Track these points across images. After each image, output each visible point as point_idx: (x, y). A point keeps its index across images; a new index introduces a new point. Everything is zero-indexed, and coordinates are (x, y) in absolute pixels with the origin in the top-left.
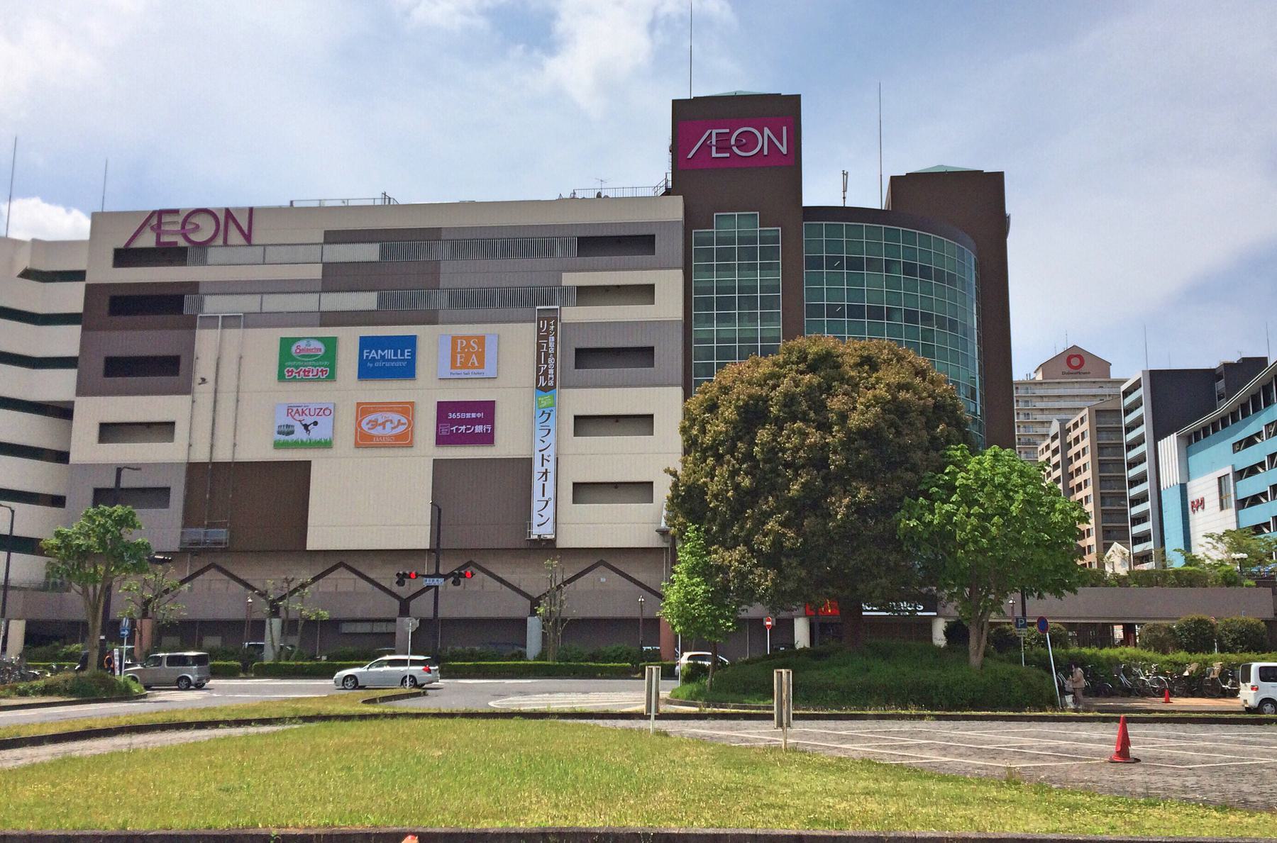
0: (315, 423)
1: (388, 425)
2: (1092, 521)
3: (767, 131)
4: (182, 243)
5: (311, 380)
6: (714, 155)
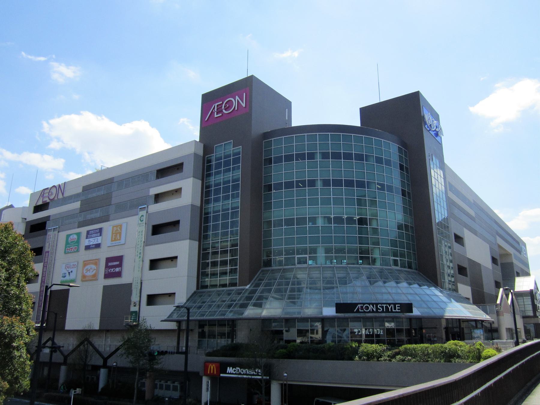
0: (72, 272)
1: (91, 271)
2: (447, 281)
3: (237, 98)
4: (48, 201)
5: (73, 252)
6: (216, 116)
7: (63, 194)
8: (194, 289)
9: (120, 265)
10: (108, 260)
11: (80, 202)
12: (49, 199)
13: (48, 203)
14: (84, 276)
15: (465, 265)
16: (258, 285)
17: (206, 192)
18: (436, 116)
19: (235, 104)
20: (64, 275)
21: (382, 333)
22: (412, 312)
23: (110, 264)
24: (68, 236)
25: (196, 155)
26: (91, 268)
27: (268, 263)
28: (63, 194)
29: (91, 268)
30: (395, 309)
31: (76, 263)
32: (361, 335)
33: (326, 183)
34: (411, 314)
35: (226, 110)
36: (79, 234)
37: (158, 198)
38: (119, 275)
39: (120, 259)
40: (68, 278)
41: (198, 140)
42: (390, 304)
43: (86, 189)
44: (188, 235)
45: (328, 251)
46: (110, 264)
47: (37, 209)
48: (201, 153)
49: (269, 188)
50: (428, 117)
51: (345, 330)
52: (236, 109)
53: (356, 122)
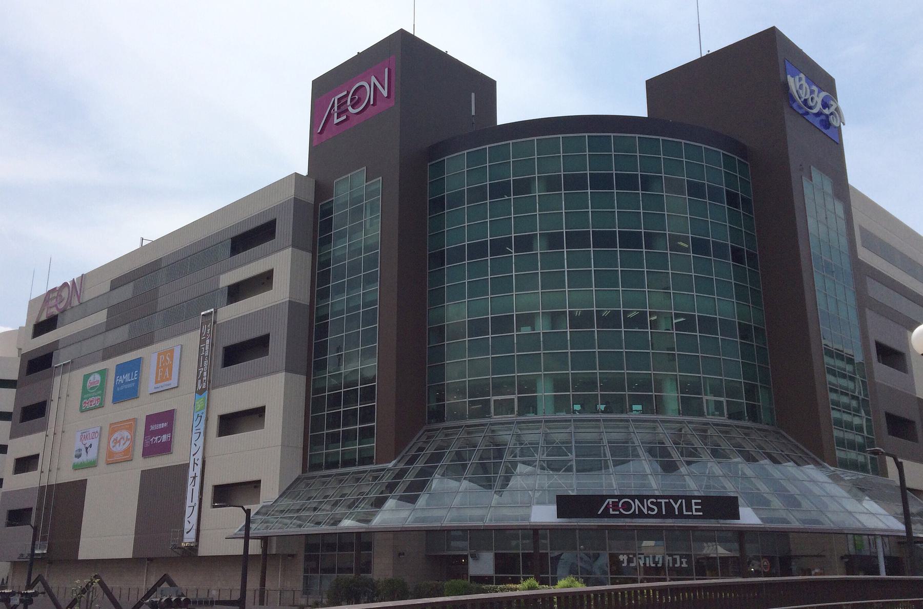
0: (91, 446)
1: (122, 442)
6: (336, 121)
7: (79, 297)
8: (298, 471)
9: (169, 430)
10: (151, 419)
11: (105, 311)
12: (58, 309)
13: (57, 316)
14: (110, 454)
15: (912, 414)
16: (412, 461)
17: (321, 277)
18: (826, 83)
19: (369, 93)
20: (78, 453)
21: (684, 565)
22: (736, 516)
23: (153, 428)
24: (86, 377)
25: (297, 202)
26: (122, 438)
27: (438, 415)
28: (79, 297)
29: (122, 438)
30: (689, 508)
31: (99, 430)
32: (635, 569)
33: (554, 241)
34: (736, 521)
35: (353, 107)
36: (103, 373)
37: (236, 292)
38: (166, 448)
39: (168, 417)
40: (84, 458)
41: (304, 172)
42: (676, 498)
43: (116, 284)
44: (282, 363)
45: (560, 384)
46: (153, 428)
47: (42, 327)
48: (310, 198)
49: (439, 258)
50: (797, 84)
51: (596, 557)
52: (372, 103)
53: (638, 108)
